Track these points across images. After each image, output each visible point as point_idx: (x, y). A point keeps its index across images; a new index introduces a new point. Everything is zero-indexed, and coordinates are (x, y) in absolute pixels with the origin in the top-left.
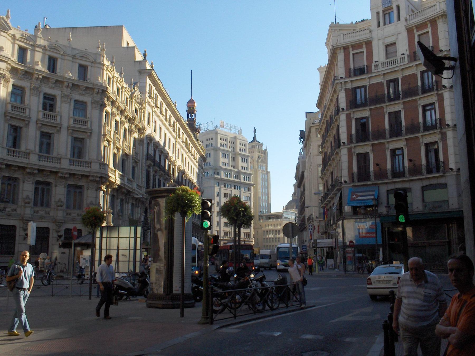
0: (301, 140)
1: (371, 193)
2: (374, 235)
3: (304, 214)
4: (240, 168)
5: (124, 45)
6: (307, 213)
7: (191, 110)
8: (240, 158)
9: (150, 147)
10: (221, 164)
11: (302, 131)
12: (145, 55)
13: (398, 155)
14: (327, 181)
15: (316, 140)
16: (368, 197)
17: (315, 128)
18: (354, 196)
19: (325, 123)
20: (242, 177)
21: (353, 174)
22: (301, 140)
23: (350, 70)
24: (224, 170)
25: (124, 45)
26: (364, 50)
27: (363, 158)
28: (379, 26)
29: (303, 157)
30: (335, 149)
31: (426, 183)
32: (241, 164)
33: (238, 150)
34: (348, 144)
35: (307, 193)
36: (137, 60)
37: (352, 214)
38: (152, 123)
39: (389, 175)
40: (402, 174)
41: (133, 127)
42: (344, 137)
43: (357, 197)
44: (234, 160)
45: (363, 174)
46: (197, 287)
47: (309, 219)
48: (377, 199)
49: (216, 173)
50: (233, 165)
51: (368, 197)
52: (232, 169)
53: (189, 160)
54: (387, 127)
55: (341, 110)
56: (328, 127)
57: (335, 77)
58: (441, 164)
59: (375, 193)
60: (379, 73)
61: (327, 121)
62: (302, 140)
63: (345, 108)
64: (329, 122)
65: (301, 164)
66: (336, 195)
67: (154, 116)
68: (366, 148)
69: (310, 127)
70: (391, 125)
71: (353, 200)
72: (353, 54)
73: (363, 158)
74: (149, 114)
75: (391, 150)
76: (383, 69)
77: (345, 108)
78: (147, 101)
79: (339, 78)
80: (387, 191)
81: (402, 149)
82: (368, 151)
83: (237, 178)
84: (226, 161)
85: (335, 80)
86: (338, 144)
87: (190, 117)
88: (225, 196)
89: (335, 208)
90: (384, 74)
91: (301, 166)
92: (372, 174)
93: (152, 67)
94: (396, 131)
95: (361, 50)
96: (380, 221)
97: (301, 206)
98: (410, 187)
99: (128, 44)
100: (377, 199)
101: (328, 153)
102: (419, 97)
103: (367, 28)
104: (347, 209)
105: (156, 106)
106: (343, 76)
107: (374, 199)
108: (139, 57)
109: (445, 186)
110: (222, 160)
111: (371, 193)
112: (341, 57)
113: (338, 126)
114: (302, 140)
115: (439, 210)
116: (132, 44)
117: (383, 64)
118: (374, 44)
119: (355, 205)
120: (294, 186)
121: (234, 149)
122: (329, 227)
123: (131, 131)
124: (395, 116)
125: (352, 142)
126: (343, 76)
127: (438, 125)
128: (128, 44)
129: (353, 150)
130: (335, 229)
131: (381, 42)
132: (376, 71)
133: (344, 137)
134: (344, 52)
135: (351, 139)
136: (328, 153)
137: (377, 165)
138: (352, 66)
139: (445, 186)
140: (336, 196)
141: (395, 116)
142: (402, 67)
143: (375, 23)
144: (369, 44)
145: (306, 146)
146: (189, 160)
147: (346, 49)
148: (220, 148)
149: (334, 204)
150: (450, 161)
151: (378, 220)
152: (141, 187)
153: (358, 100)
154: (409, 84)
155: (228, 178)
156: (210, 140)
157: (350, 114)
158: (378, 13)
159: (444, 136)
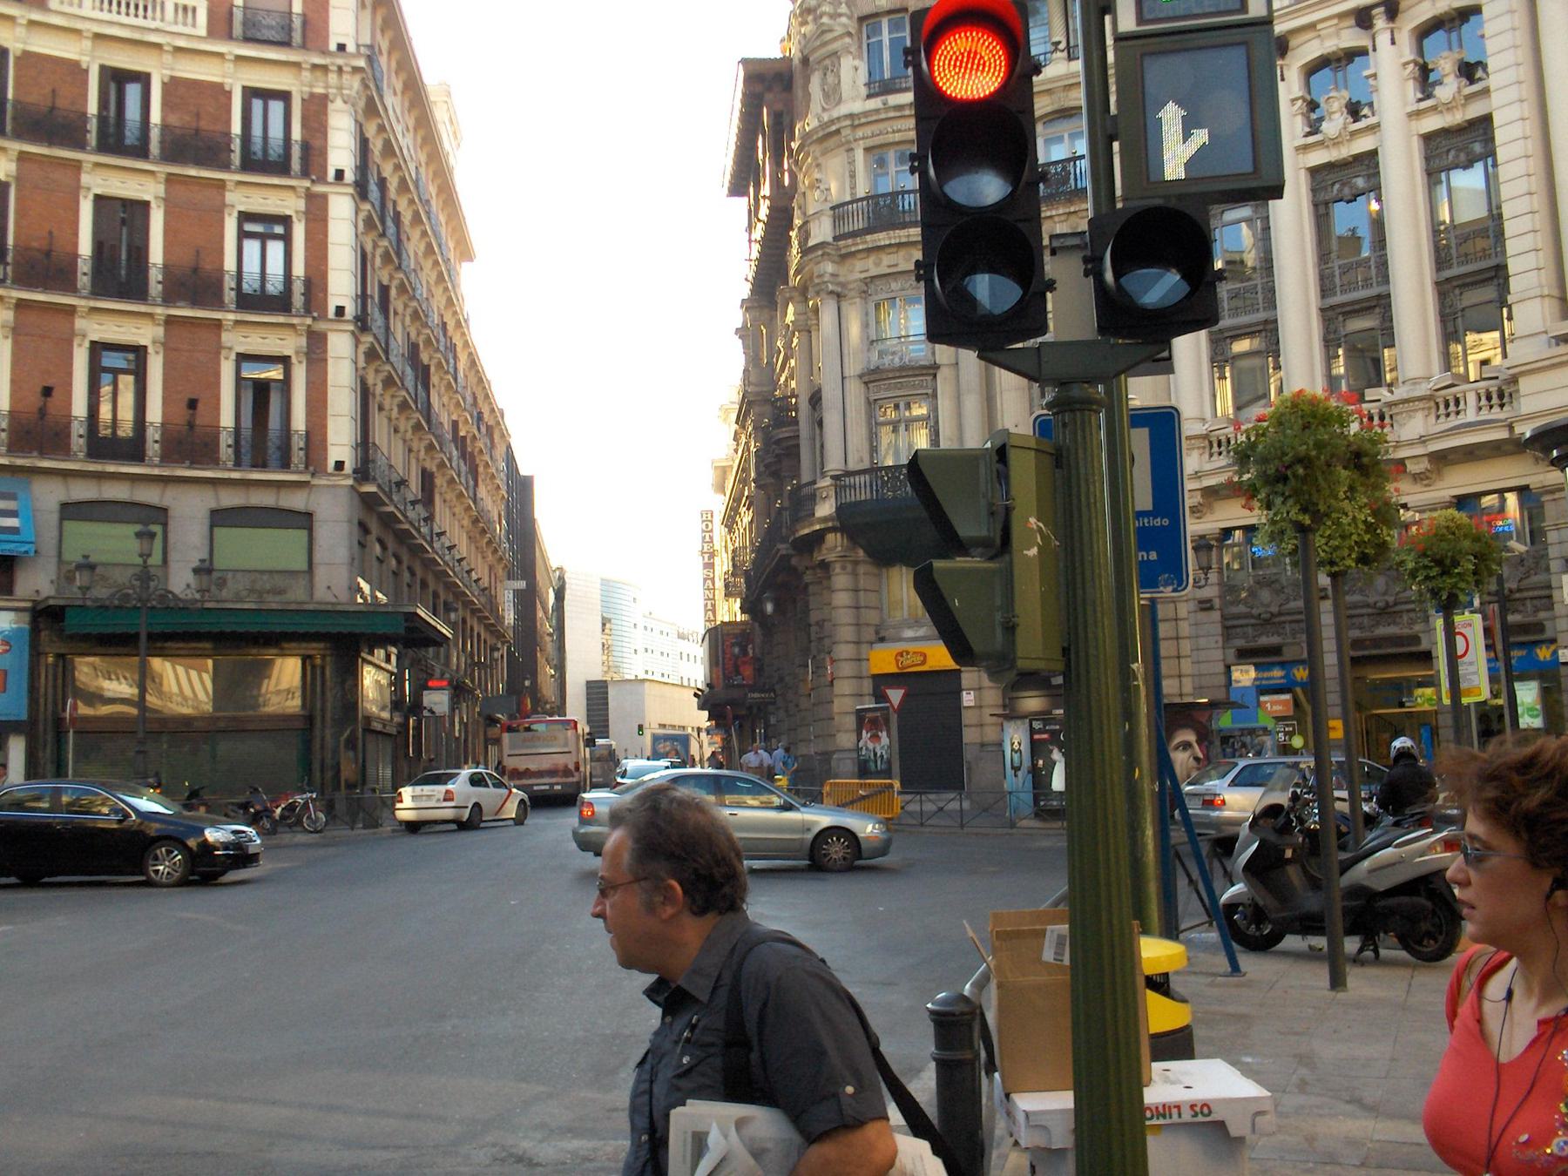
5: (1201, 137)
13: (116, 372)
25: (1201, 137)
31: (230, 499)
39: (78, 443)
40: (133, 449)
46: (947, 684)
54: (85, 247)
58: (298, 443)
60: (79, 25)
70: (98, 246)
81: (139, 352)
90: (98, 37)
94: (120, 274)
95: (1083, 206)
98: (310, 509)
109: (305, 520)
115: (273, 603)
124: (121, 218)
127: (298, 300)
139: (305, 520)
141: (121, 218)
142: (182, 43)
150: (332, 437)
153: (128, 133)
154: (198, 115)
159: (316, 346)
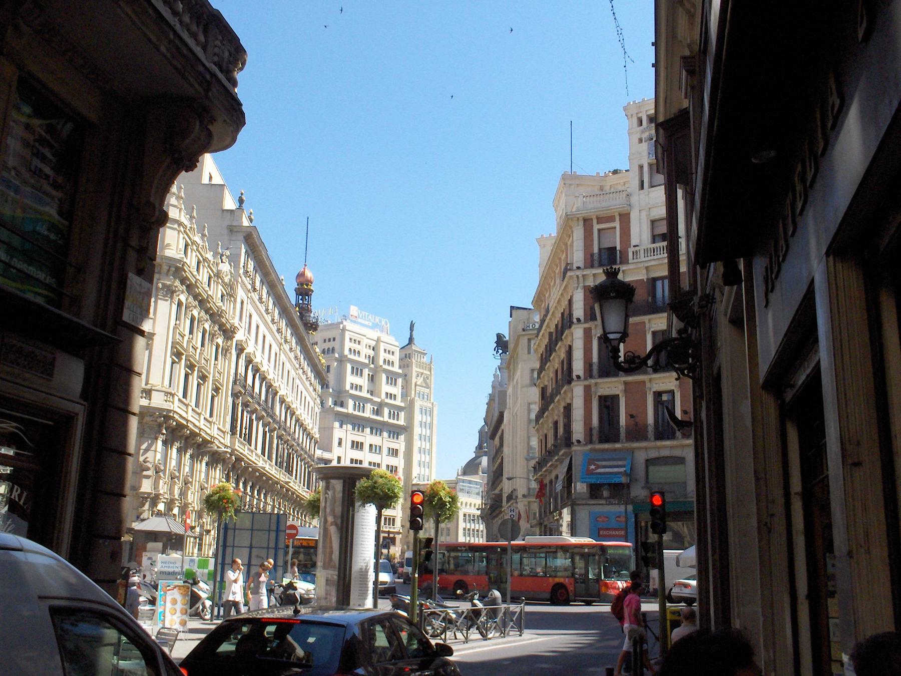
0: (497, 352)
1: (620, 463)
2: (623, 533)
3: (499, 489)
4: (383, 396)
6: (506, 487)
7: (304, 291)
8: (384, 376)
9: (240, 360)
10: (348, 387)
11: (500, 339)
12: (241, 201)
14: (546, 435)
15: (528, 363)
16: (615, 470)
17: (526, 338)
18: (593, 467)
19: (547, 336)
20: (386, 411)
21: (591, 429)
22: (497, 352)
23: (592, 255)
24: (354, 397)
25: (205, 180)
26: (617, 224)
27: (608, 404)
28: (642, 187)
29: (500, 384)
30: (563, 386)
32: (386, 388)
33: (381, 363)
34: (586, 321)
35: (506, 450)
36: (226, 208)
37: (588, 495)
38: (245, 319)
41: (216, 328)
42: (578, 367)
43: (596, 469)
44: (372, 380)
45: (608, 429)
47: (510, 498)
48: (631, 474)
49: (339, 403)
50: (371, 388)
51: (615, 470)
52: (369, 396)
53: (297, 382)
55: (575, 320)
56: (553, 346)
57: (567, 264)
59: (627, 463)
61: (551, 334)
62: (500, 351)
63: (582, 318)
64: (554, 335)
65: (497, 395)
66: (561, 461)
67: (250, 307)
68: (613, 386)
69: (519, 337)
71: (590, 473)
72: (599, 230)
73: (608, 404)
74: (242, 302)
75: (654, 392)
76: (647, 259)
77: (582, 318)
78: (240, 280)
79: (575, 268)
80: (647, 460)
81: (672, 392)
82: (617, 393)
83: (377, 414)
84: (357, 380)
85: (566, 270)
86: (566, 376)
87: (301, 302)
88: (352, 447)
89: (559, 486)
91: (497, 399)
92: (623, 431)
93: (251, 220)
96: (634, 510)
97: (494, 473)
99: (211, 178)
100: (631, 474)
101: (549, 390)
102: (644, 444)
103: (620, 188)
104: (580, 487)
105: (255, 290)
106: (582, 266)
107: (625, 474)
108: (229, 204)
110: (351, 379)
111: (620, 463)
112: (578, 233)
113: (570, 347)
114: (500, 351)
116: (217, 180)
117: (646, 251)
118: (634, 216)
119: (593, 481)
120: (481, 432)
121: (373, 360)
122: (546, 516)
123: (213, 336)
125: (591, 377)
126: (582, 266)
128: (211, 178)
129: (593, 389)
130: (557, 520)
131: (644, 214)
132: (635, 261)
133: (578, 367)
134: (584, 225)
135: (591, 435)
136: (549, 390)
137: (632, 416)
138: (596, 250)
140: (562, 463)
143: (636, 183)
144: (625, 218)
145: (508, 367)
146: (297, 382)
147: (587, 222)
148: (349, 356)
149: (557, 477)
151: (630, 508)
152: (224, 432)
155: (361, 414)
156: (329, 340)
157: (590, 329)
158: (641, 167)
